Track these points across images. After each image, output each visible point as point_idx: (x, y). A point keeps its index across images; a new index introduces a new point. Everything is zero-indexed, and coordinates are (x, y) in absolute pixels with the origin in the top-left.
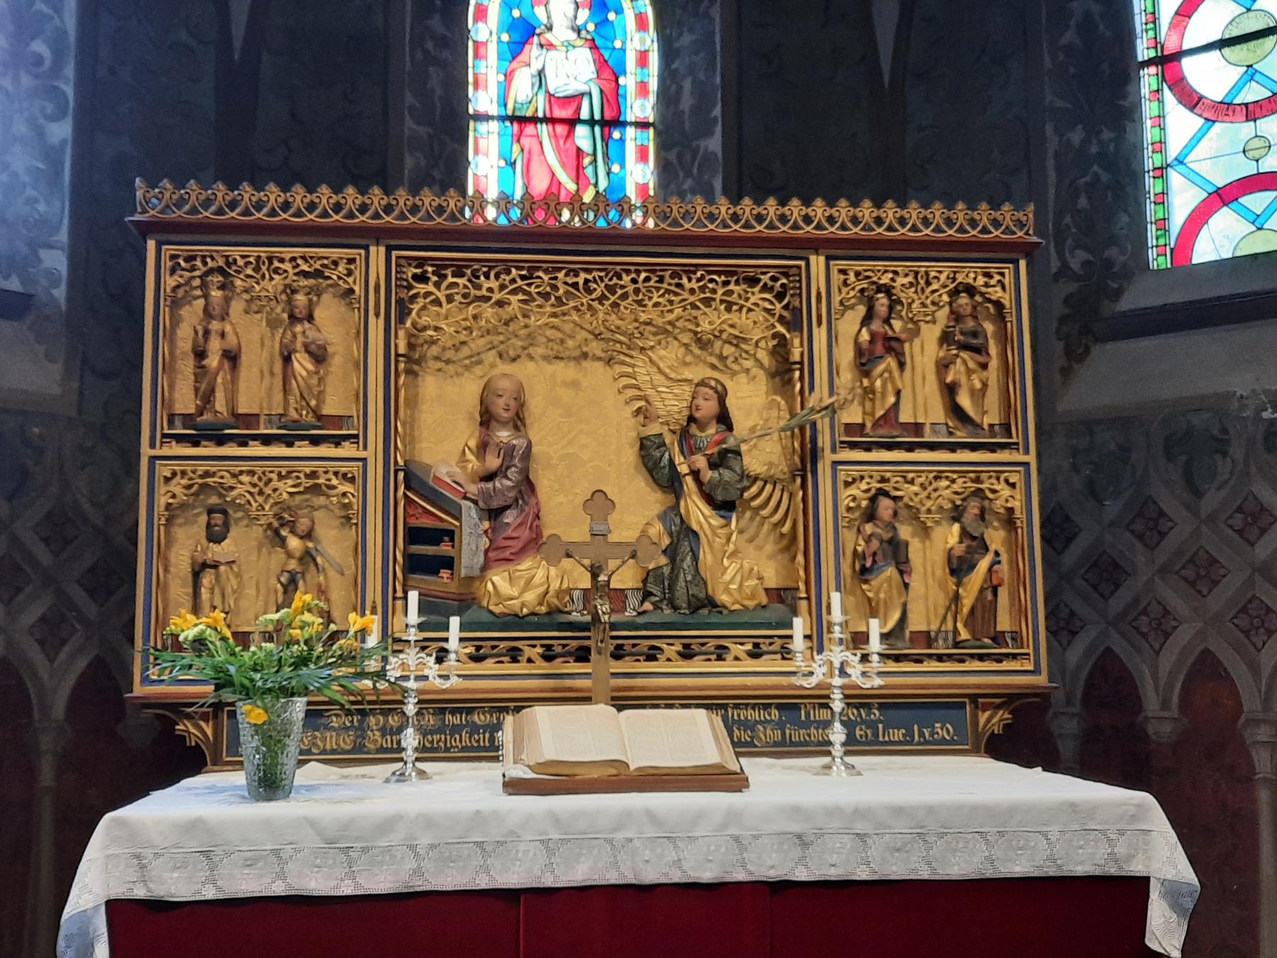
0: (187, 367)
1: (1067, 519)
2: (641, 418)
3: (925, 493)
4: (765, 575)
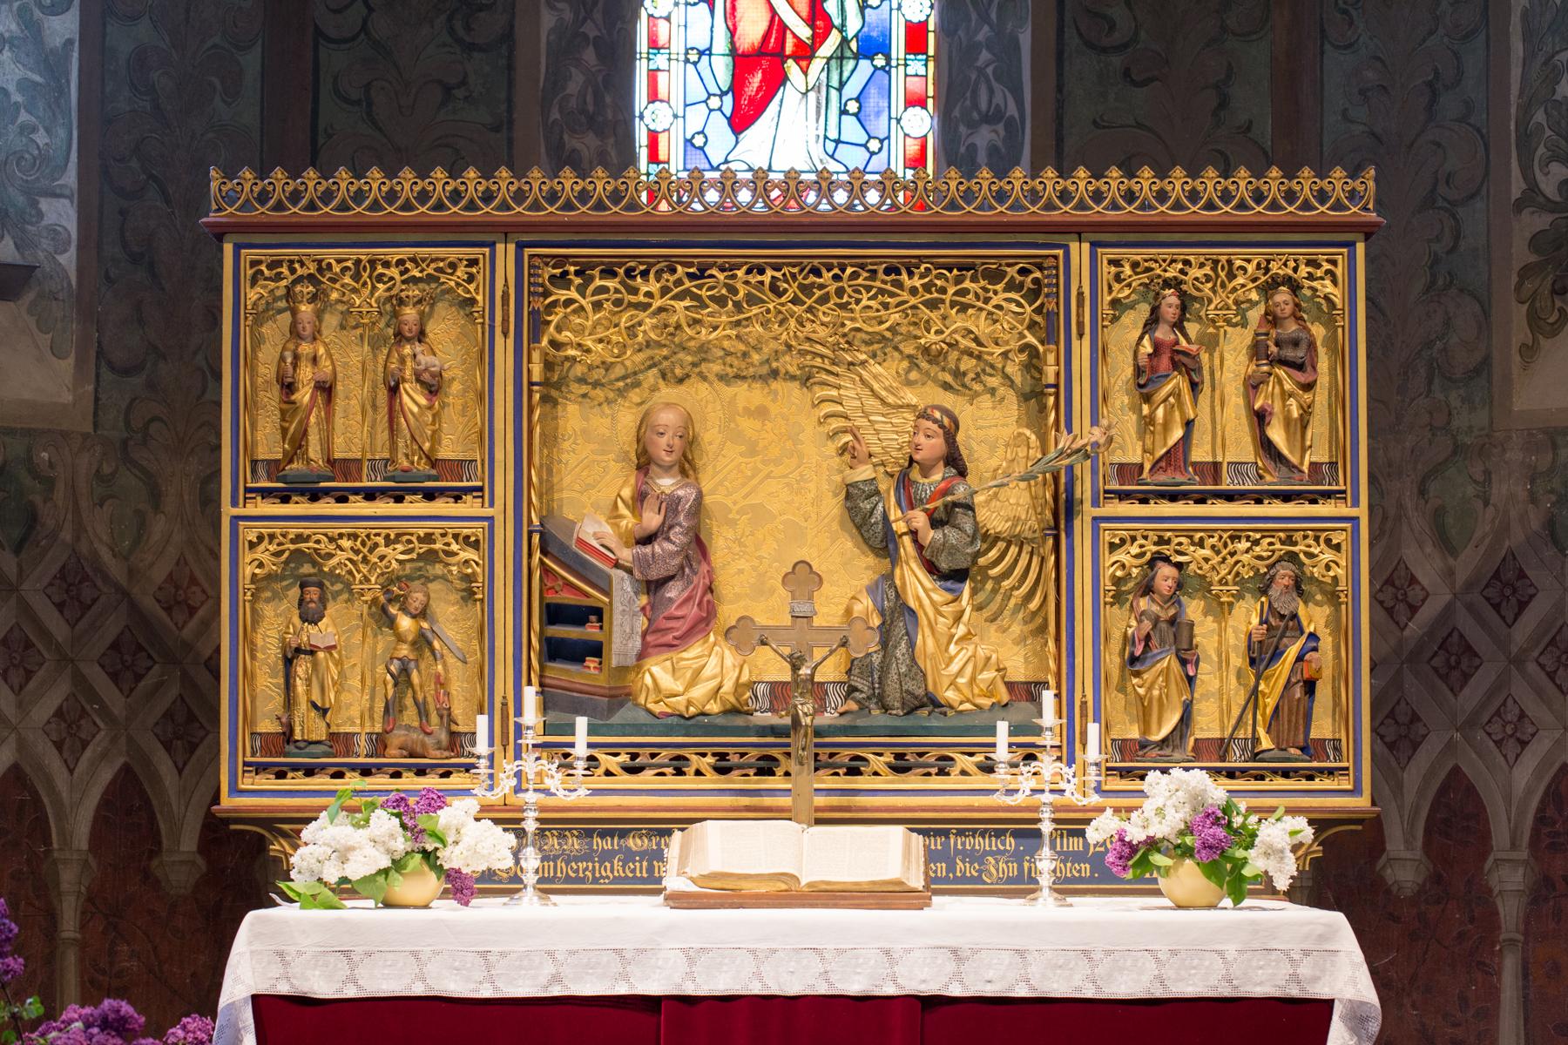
0: (270, 399)
1: (1522, 575)
2: (847, 457)
3: (1219, 559)
4: (1007, 664)
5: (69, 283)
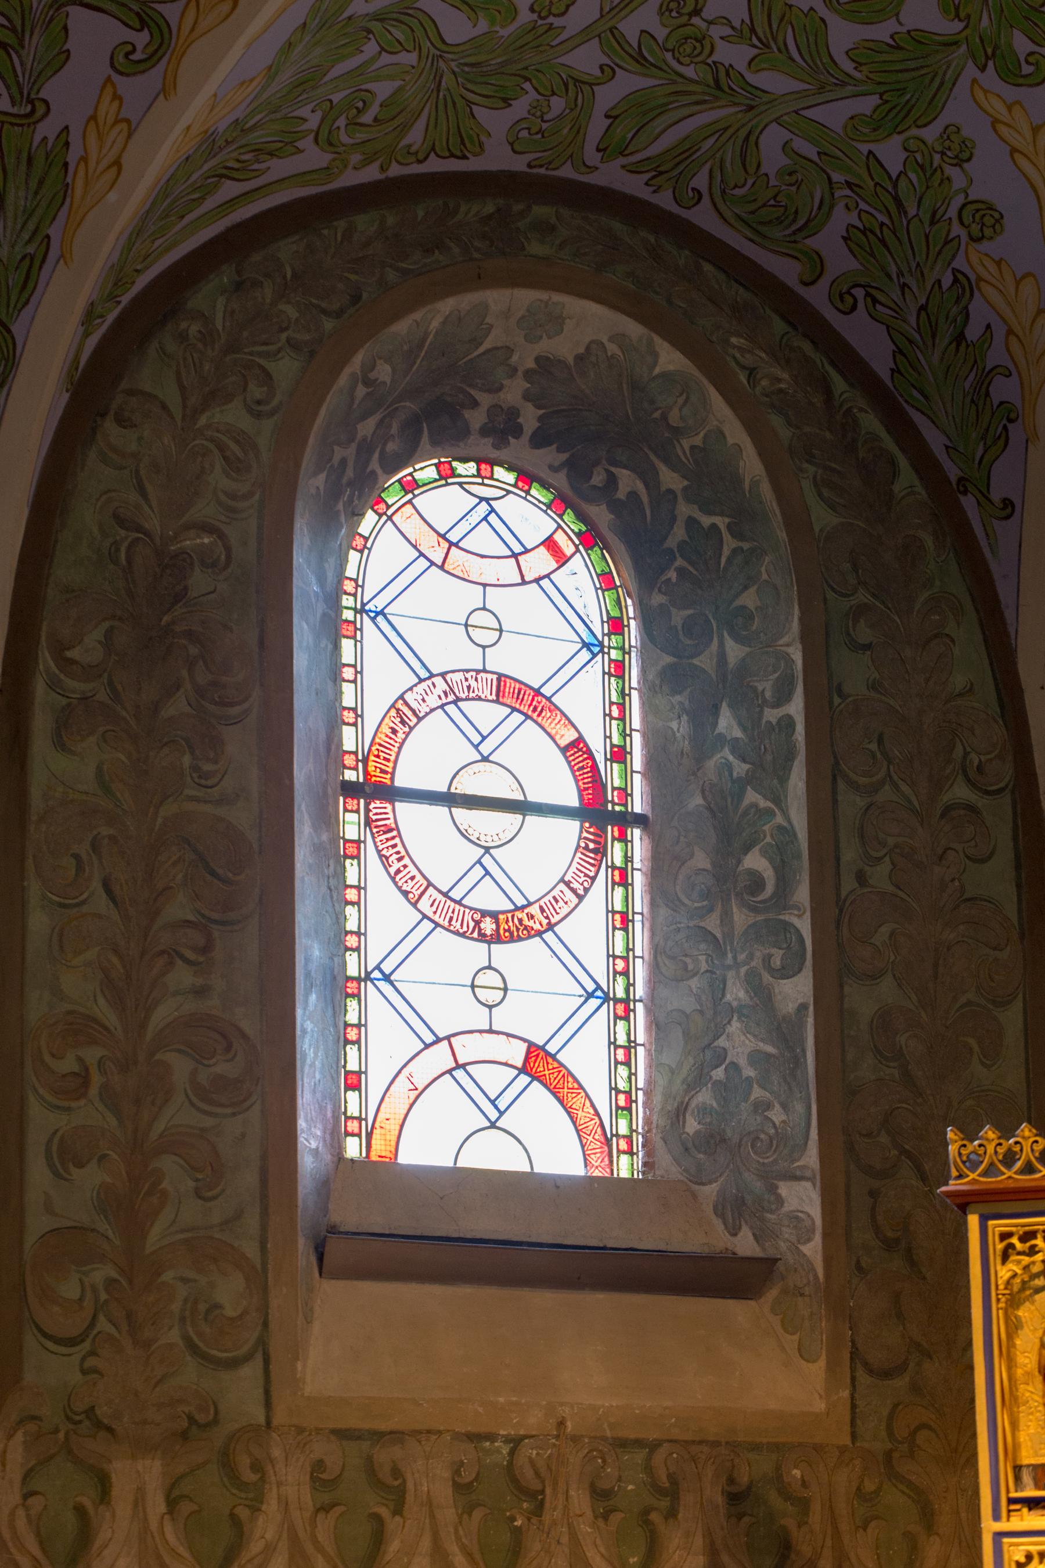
5: (816, 1276)
